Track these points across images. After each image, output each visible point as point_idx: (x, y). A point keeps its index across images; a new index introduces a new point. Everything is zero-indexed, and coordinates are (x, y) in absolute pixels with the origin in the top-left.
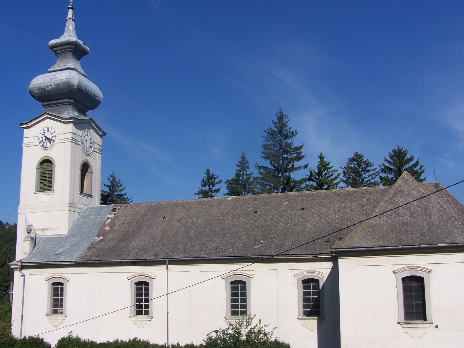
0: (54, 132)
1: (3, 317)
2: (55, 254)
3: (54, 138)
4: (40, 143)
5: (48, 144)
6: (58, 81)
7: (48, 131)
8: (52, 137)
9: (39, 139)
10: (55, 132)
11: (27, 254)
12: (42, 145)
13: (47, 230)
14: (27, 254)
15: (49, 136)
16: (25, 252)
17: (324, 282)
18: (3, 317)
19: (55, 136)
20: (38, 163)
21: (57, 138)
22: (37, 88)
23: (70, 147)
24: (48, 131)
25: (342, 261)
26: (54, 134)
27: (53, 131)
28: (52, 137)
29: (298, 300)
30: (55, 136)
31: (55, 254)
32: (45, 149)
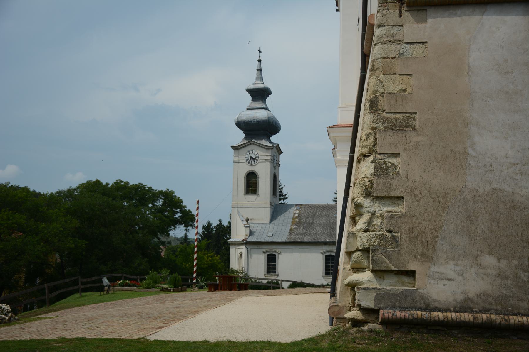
0: (257, 154)
1: (484, 213)
2: (268, 236)
3: (257, 158)
4: (246, 160)
5: (253, 162)
6: (260, 119)
7: (253, 153)
8: (256, 157)
9: (245, 158)
10: (257, 154)
11: (247, 235)
12: (248, 162)
13: (254, 220)
14: (247, 235)
15: (254, 157)
16: (246, 234)
17: (152, 338)
18: (484, 213)
19: (258, 157)
20: (245, 175)
21: (260, 158)
22: (243, 122)
23: (270, 165)
24: (253, 153)
25: (283, 282)
26: (257, 156)
27: (256, 153)
28: (256, 157)
29: (335, 284)
30: (258, 157)
31: (268, 236)
32: (251, 165)
